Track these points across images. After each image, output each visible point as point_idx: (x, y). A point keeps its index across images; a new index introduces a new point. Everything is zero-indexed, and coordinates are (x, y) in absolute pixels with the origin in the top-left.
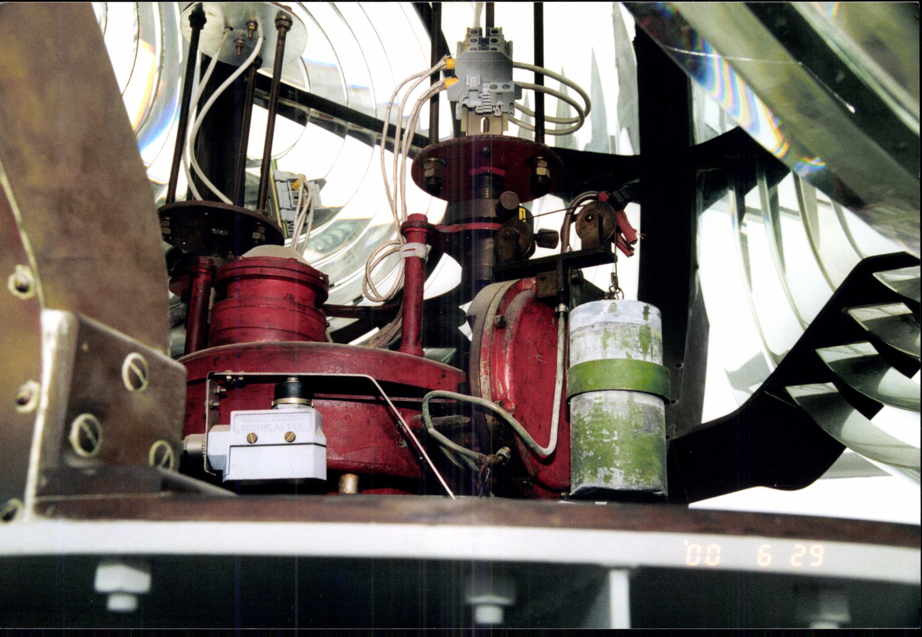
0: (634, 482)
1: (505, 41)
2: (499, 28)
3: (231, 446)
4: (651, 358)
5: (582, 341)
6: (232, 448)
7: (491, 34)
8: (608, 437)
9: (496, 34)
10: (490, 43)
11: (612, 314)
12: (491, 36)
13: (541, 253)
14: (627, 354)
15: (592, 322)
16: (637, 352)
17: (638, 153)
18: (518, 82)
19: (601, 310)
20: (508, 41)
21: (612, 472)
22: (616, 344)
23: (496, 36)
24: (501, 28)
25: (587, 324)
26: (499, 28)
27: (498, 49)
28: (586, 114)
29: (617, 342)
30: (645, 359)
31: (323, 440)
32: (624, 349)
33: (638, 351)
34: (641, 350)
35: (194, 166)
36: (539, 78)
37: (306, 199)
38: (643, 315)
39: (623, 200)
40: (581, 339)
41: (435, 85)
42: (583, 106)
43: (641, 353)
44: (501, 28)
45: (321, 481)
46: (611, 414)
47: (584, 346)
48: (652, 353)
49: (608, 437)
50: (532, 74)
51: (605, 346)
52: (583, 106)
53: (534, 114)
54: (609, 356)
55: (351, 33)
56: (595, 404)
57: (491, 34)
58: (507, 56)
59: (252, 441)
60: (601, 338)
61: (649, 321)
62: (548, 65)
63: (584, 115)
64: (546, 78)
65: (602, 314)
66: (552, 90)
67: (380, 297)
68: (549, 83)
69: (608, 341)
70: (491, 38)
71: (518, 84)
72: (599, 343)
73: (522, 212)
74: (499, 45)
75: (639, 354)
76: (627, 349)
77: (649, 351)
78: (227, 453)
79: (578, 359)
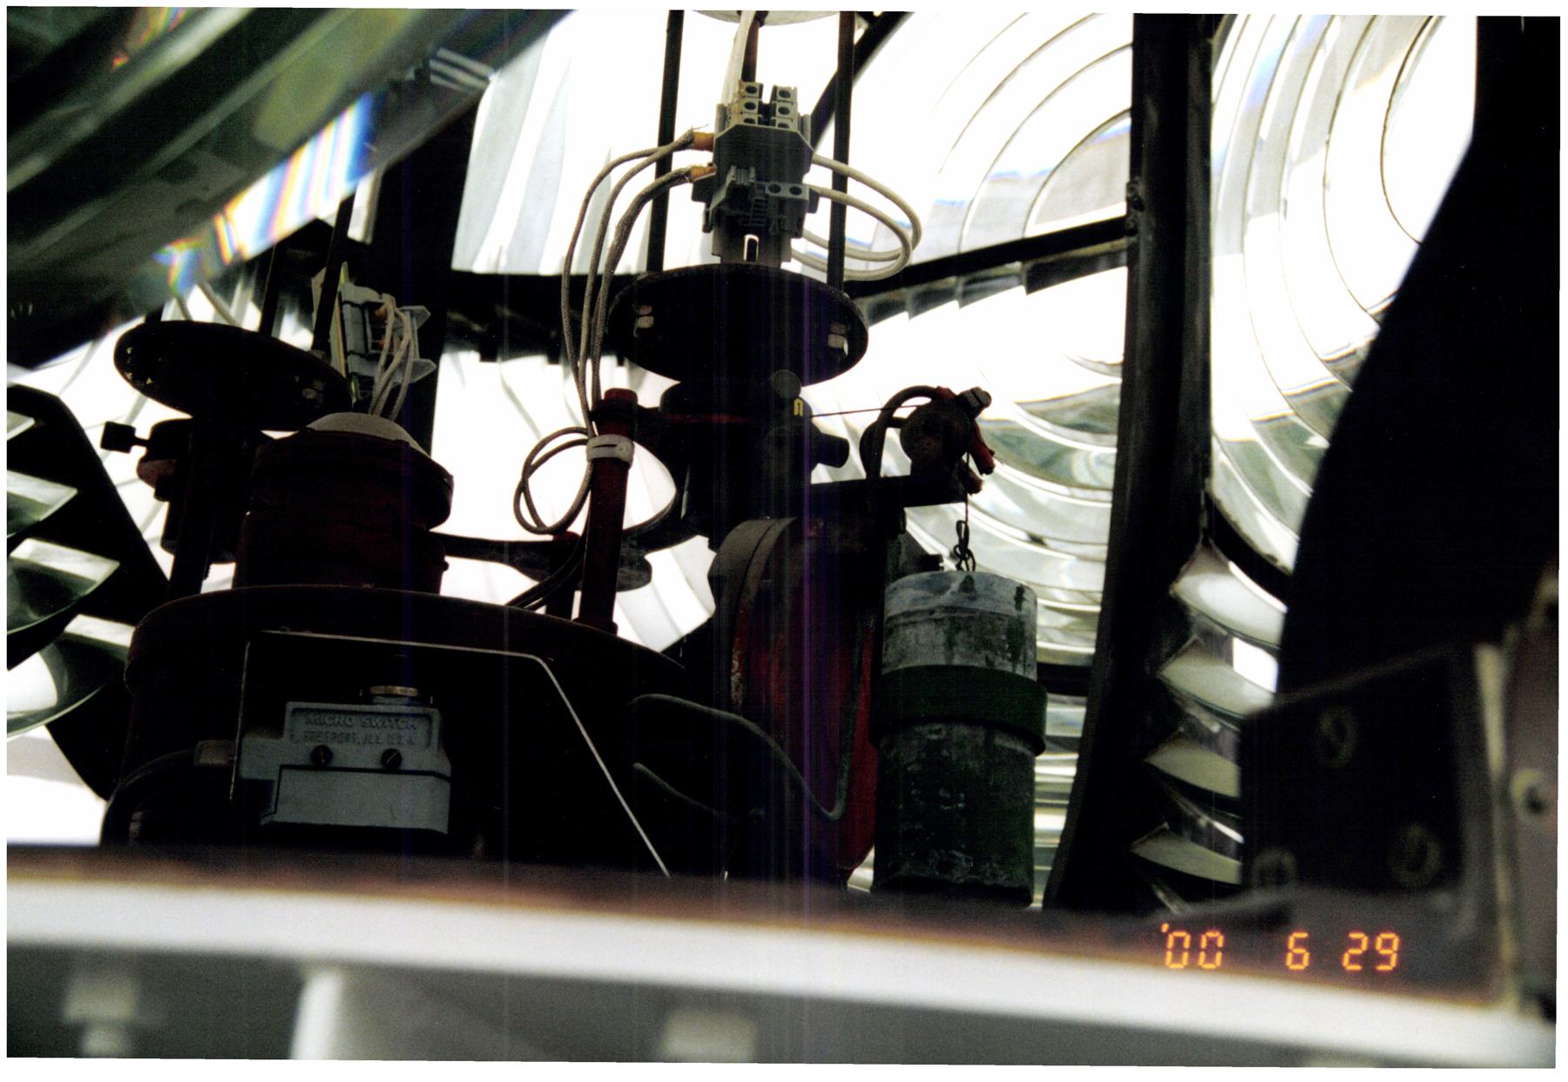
0: (987, 874)
1: (799, 114)
2: (793, 88)
3: (283, 767)
4: (1022, 669)
5: (911, 633)
6: (285, 772)
7: (779, 97)
8: (947, 802)
9: (788, 99)
10: (778, 113)
11: (965, 594)
12: (779, 101)
13: (821, 474)
14: (987, 659)
15: (932, 604)
16: (1004, 659)
17: (369, 241)
18: (814, 187)
19: (948, 587)
20: (802, 115)
21: (954, 857)
22: (969, 643)
23: (787, 102)
24: (796, 89)
25: (921, 607)
26: (793, 88)
27: (791, 126)
28: (914, 247)
29: (972, 639)
30: (1014, 670)
31: (445, 767)
32: (983, 652)
33: (1004, 658)
34: (1009, 655)
35: (1062, 489)
36: (840, 181)
37: (400, 343)
38: (1014, 602)
39: (978, 404)
40: (908, 631)
41: (663, 178)
42: (909, 234)
43: (1010, 660)
44: (796, 89)
45: (443, 834)
46: (955, 763)
47: (914, 642)
48: (1024, 661)
49: (947, 802)
50: (829, 173)
51: (950, 644)
52: (909, 234)
53: (827, 245)
54: (957, 661)
55: (1007, 25)
56: (929, 740)
57: (779, 97)
58: (801, 135)
59: (321, 760)
60: (945, 632)
61: (1023, 612)
62: (856, 162)
63: (911, 245)
64: (851, 182)
65: (948, 593)
66: (868, 206)
67: (544, 526)
68: (854, 189)
69: (956, 636)
70: (779, 105)
71: (814, 189)
72: (941, 638)
73: (799, 404)
74: (792, 121)
75: (1006, 661)
76: (988, 652)
77: (1021, 658)
78: (275, 778)
79: (900, 661)
